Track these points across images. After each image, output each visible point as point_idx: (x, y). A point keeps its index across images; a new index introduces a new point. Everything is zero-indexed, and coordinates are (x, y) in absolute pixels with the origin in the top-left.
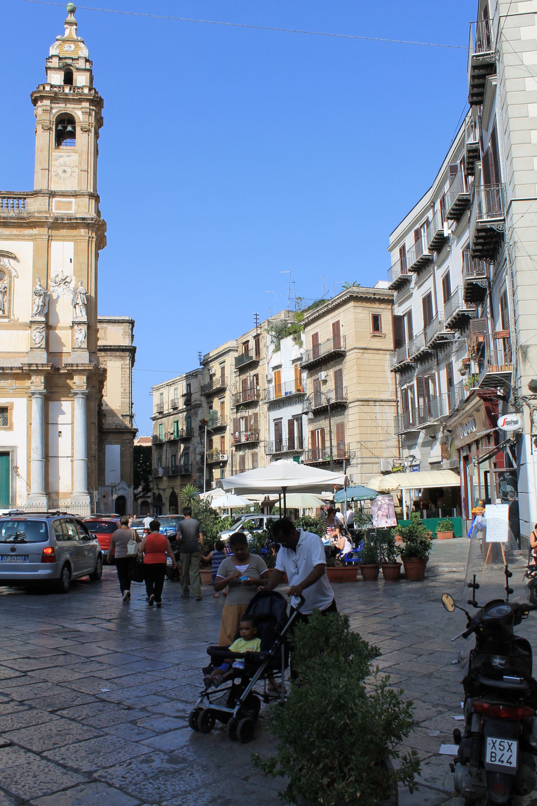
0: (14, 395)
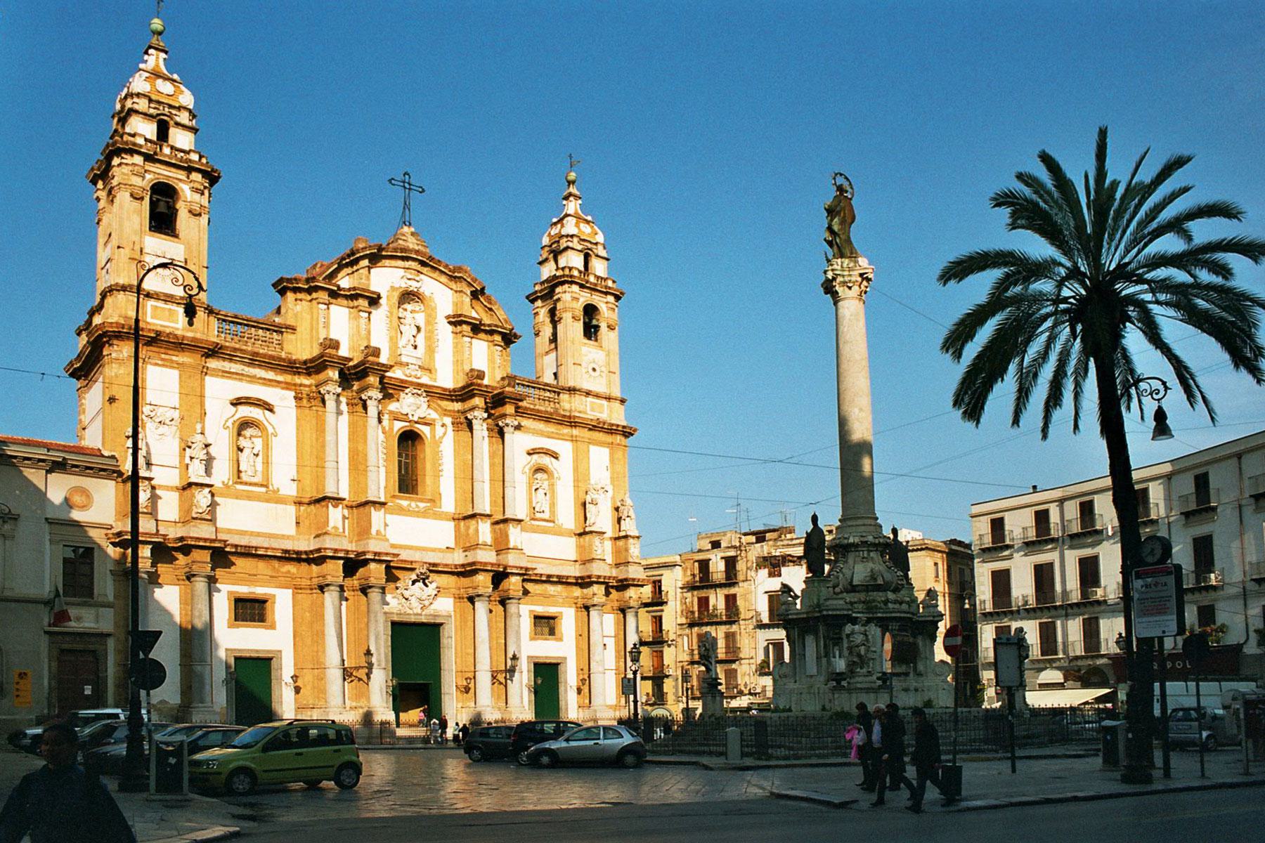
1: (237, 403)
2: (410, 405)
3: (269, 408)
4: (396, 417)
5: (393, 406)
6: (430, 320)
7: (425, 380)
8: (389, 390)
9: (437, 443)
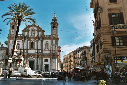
0: (48, 58)
1: (45, 42)
2: (32, 39)
3: (19, 42)
4: (30, 41)
5: (30, 40)
6: (35, 31)
7: (34, 37)
8: (31, 38)
9: (35, 43)
